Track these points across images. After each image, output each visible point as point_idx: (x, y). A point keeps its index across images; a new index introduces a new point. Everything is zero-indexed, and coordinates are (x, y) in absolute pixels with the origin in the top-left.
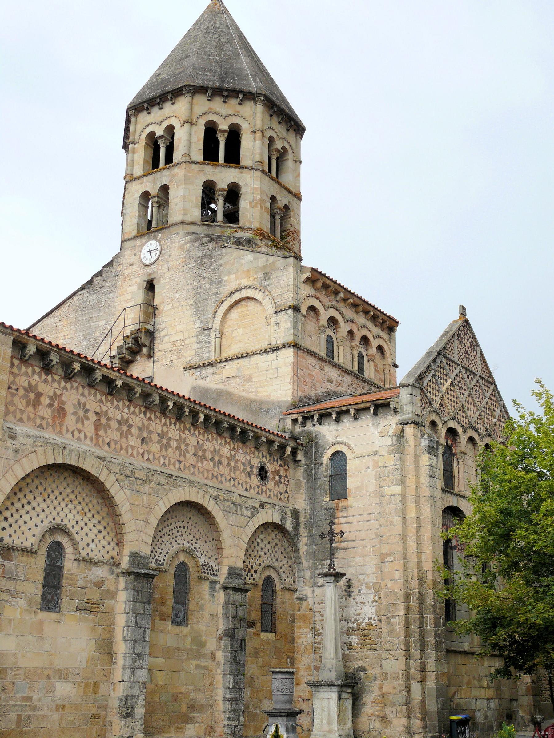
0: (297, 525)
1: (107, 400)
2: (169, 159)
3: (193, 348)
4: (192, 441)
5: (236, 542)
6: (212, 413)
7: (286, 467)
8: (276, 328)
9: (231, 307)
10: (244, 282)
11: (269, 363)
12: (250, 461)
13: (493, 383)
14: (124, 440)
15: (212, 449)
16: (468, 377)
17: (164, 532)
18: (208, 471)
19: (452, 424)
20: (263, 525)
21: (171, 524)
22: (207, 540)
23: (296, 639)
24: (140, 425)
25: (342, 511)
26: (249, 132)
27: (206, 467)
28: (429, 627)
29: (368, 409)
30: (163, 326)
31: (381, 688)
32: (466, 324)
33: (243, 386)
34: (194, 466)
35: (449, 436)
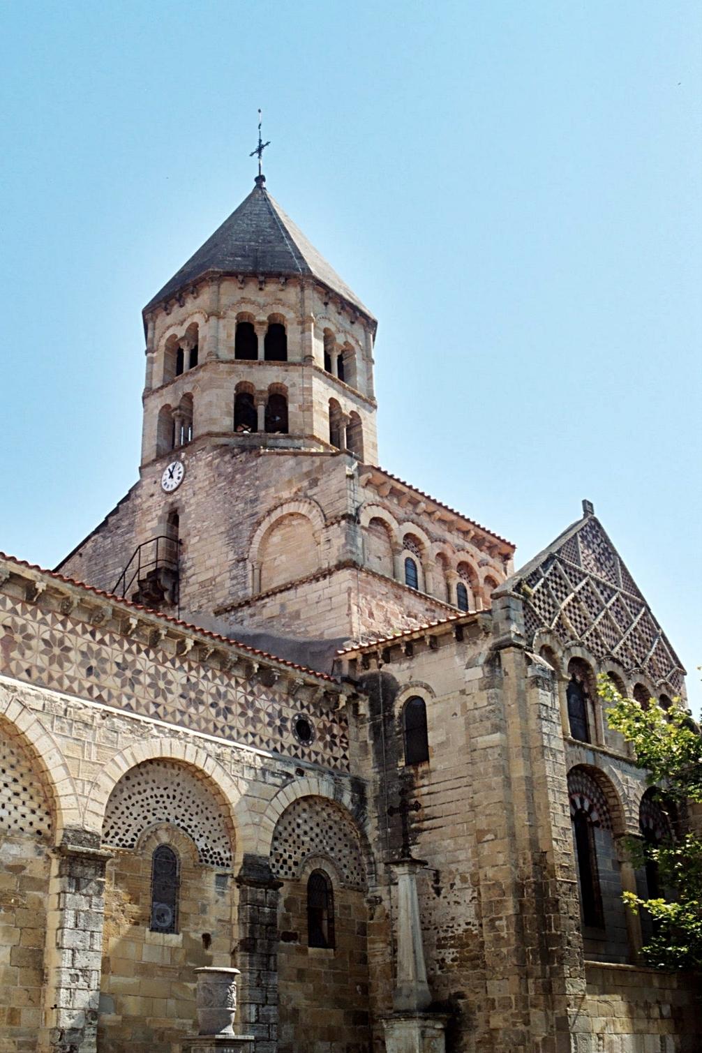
0: (361, 802)
1: (25, 611)
2: (194, 362)
3: (226, 586)
4: (179, 677)
5: (257, 820)
6: (207, 640)
7: (343, 724)
8: (327, 547)
9: (272, 529)
10: (286, 494)
11: (321, 592)
12: (280, 712)
13: (644, 604)
14: (55, 667)
15: (214, 691)
16: (602, 593)
17: (133, 800)
18: (207, 721)
19: (578, 652)
20: (305, 799)
21: (145, 791)
22: (210, 815)
23: (370, 959)
24: (84, 649)
25: (422, 778)
26: (296, 323)
27: (204, 715)
28: (554, 931)
29: (448, 633)
30: (189, 564)
31: (488, 1022)
32: (595, 526)
33: (289, 626)
34: (182, 713)
35: (576, 668)
